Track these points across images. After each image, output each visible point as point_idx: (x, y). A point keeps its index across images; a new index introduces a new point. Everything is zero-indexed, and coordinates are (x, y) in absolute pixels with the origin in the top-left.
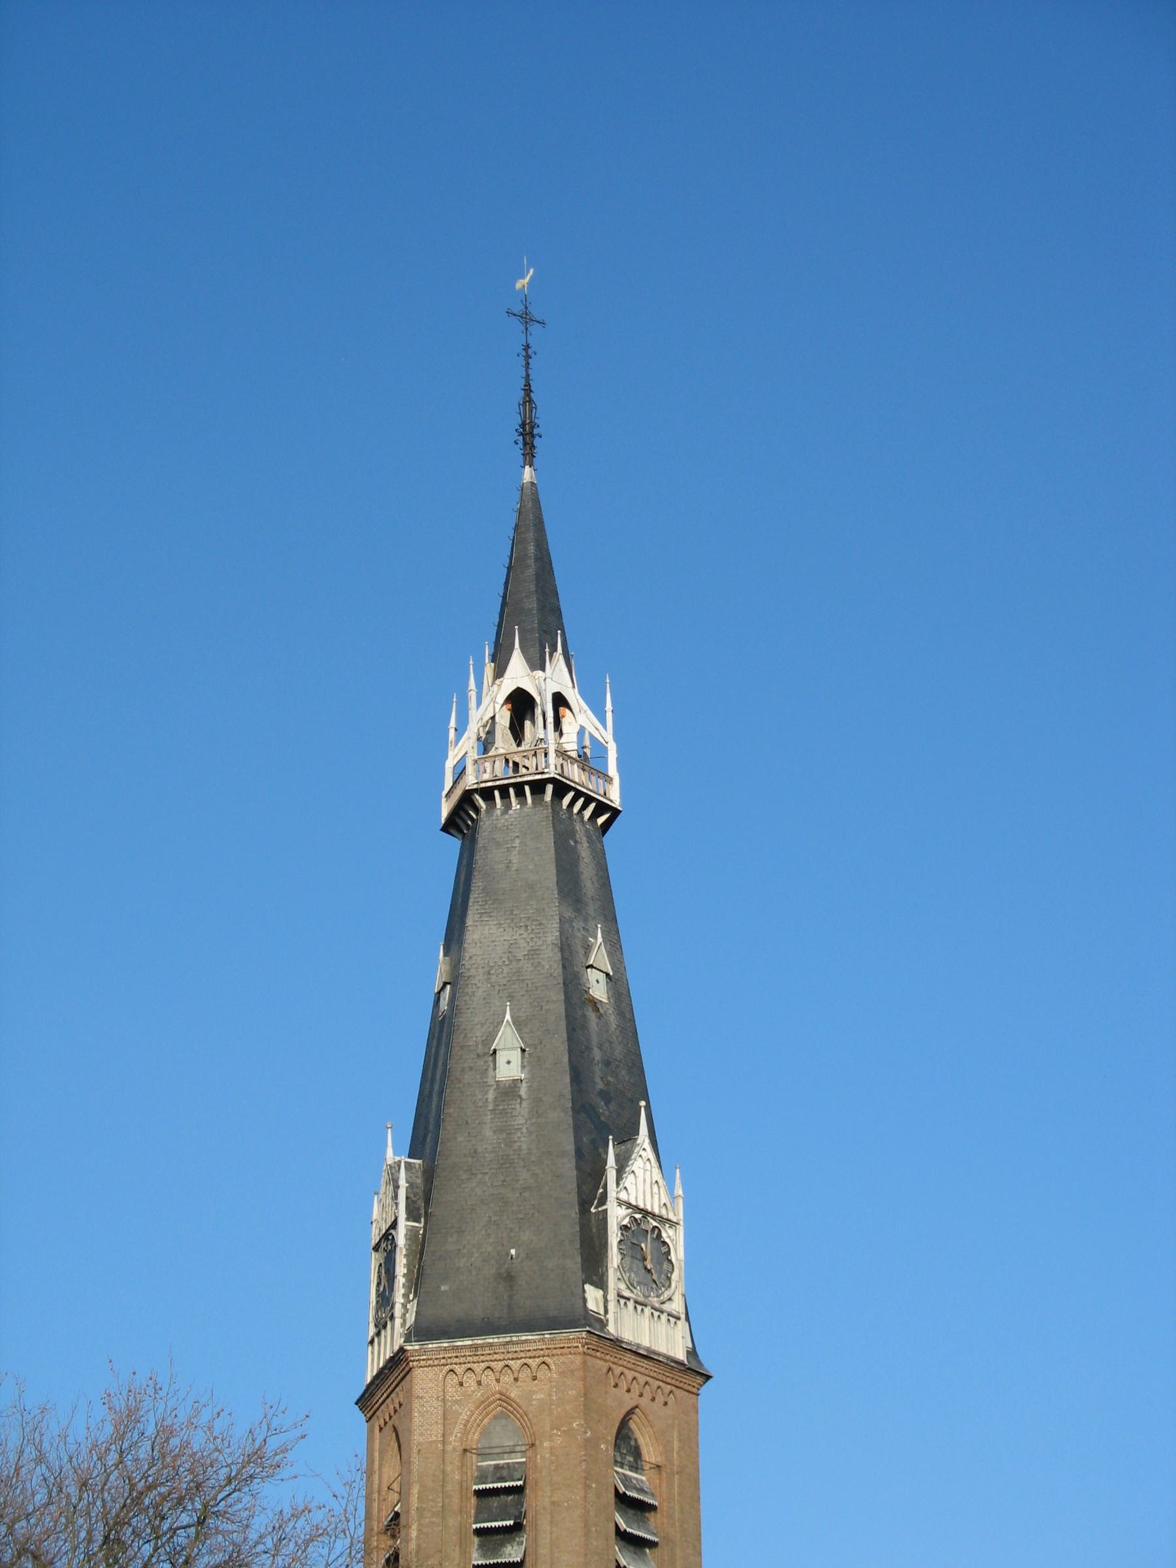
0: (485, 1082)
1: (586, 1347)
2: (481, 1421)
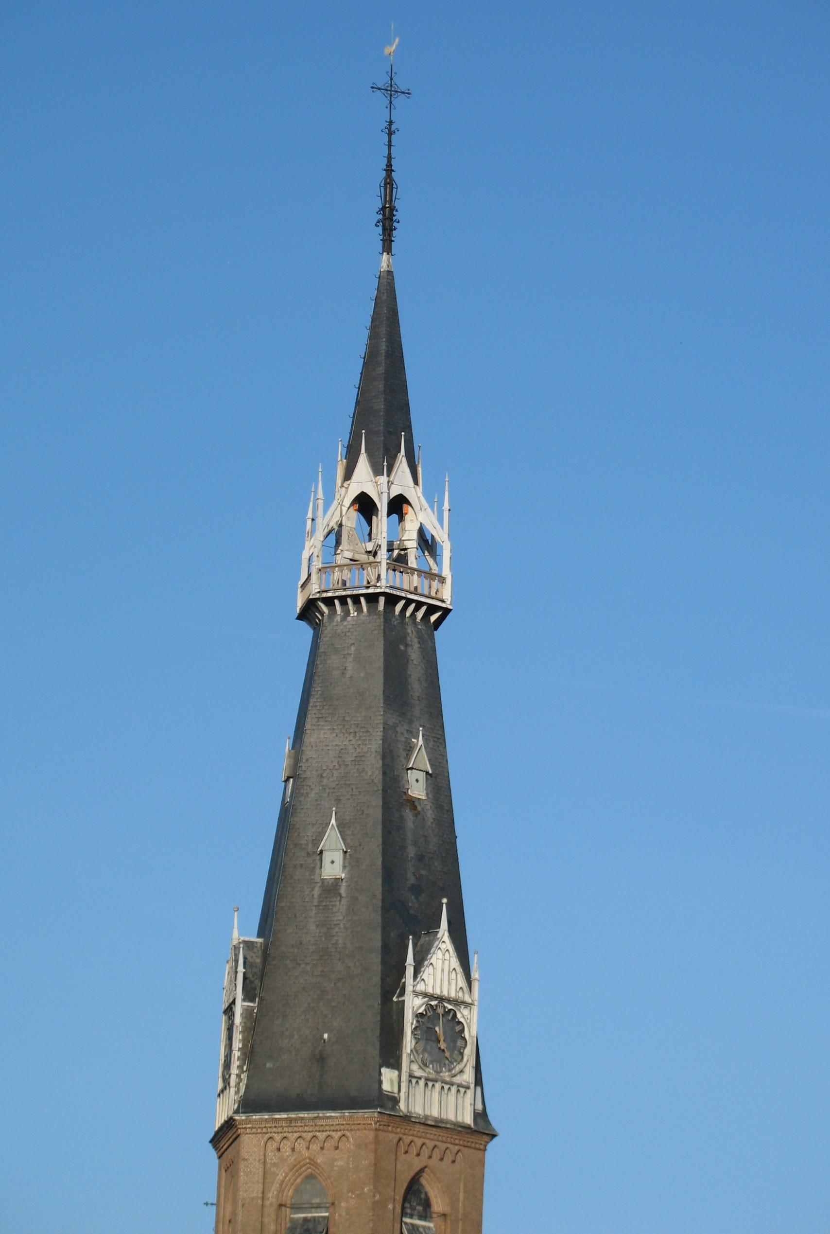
0: (312, 879)
1: (378, 1124)
2: (295, 1180)
